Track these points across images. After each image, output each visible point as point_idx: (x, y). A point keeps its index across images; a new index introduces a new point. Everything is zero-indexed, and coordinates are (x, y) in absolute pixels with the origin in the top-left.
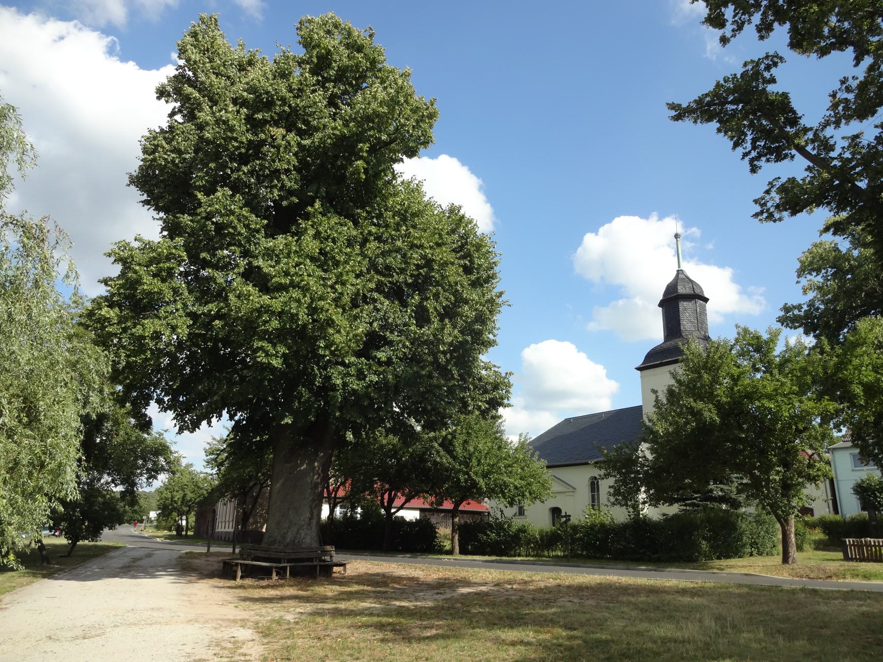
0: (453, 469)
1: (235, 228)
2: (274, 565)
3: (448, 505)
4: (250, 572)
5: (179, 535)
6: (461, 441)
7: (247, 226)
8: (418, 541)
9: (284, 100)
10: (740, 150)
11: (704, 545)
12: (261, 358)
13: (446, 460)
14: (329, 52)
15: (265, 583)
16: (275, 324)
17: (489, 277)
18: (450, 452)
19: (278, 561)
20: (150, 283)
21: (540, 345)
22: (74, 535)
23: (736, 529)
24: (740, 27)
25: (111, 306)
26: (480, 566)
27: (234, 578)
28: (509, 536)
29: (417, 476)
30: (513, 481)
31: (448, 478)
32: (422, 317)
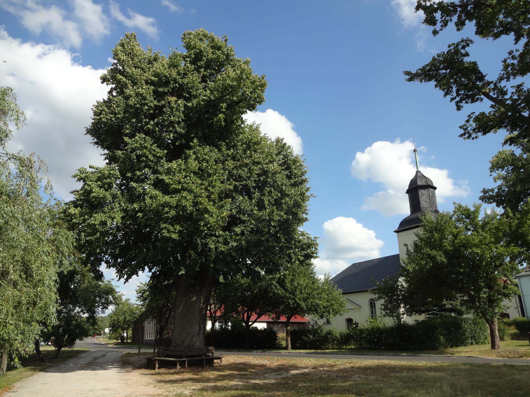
0: (285, 297)
1: (147, 157)
2: (178, 359)
3: (283, 319)
4: (164, 365)
5: (122, 342)
6: (289, 280)
8: (266, 342)
9: (175, 80)
10: (449, 97)
11: (442, 339)
12: (166, 234)
14: (201, 51)
15: (172, 371)
16: (173, 213)
19: (180, 357)
20: (97, 192)
21: (334, 220)
22: (58, 344)
25: (76, 207)
26: (304, 357)
31: (283, 303)
32: (261, 206)
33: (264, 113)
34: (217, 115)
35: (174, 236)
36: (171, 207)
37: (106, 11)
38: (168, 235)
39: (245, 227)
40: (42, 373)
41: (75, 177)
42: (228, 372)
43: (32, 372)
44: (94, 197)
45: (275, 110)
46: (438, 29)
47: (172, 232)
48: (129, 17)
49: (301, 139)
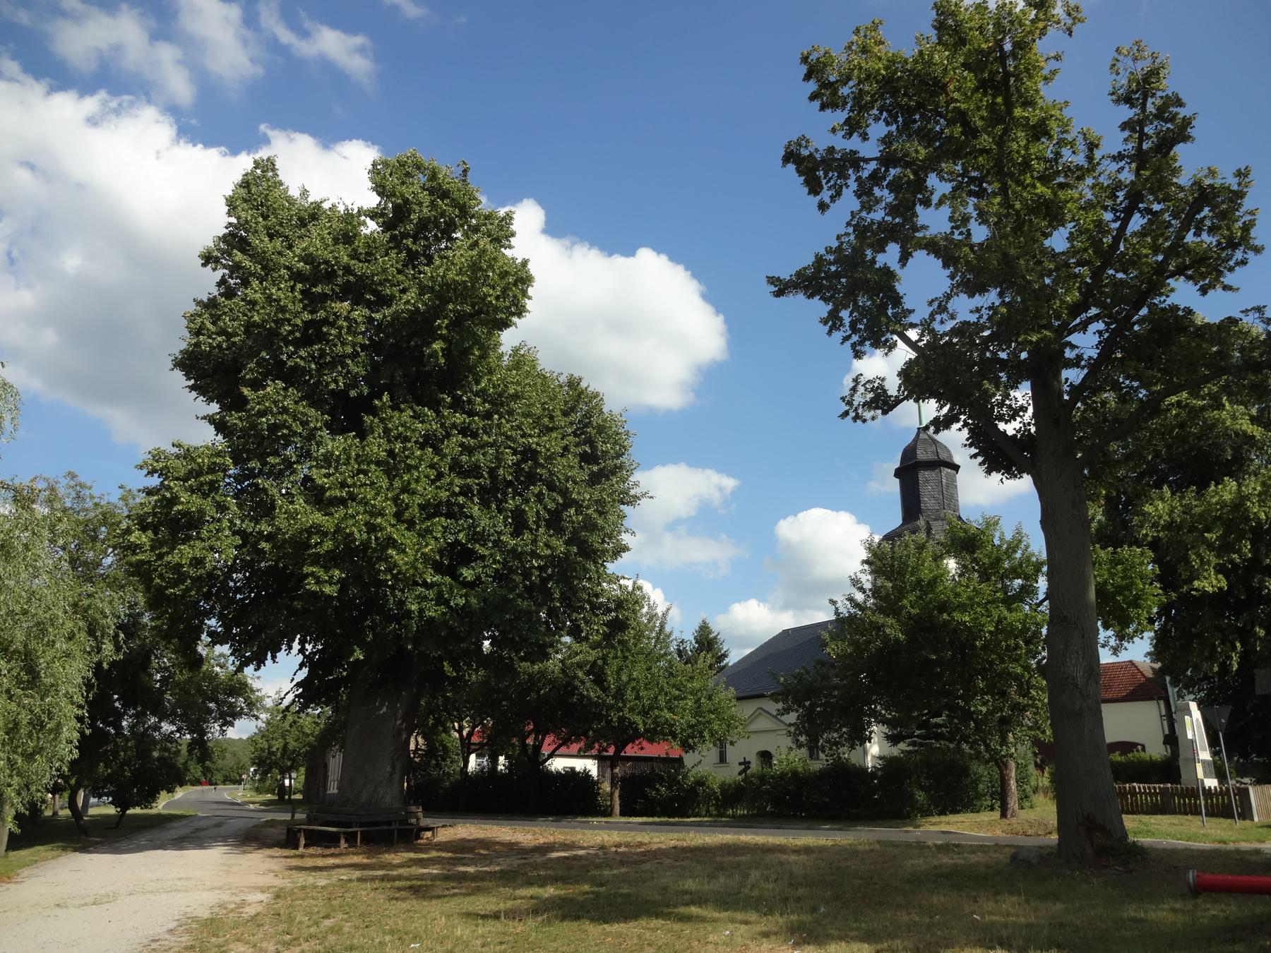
1: (289, 428)
2: (343, 830)
4: (315, 839)
5: (281, 799)
7: (304, 424)
8: (574, 798)
9: (348, 270)
10: (838, 335)
11: (920, 796)
12: (311, 585)
13: (594, 693)
14: (406, 201)
15: (332, 850)
16: (328, 545)
17: (616, 467)
18: (600, 680)
19: (349, 825)
20: (188, 501)
21: (801, 515)
22: (122, 802)
23: (968, 775)
24: (839, 193)
25: (144, 528)
26: (636, 830)
27: (297, 848)
28: (684, 790)
29: (574, 717)
30: (682, 720)
31: (598, 717)
32: (519, 524)
33: (632, 259)
34: (429, 344)
35: (327, 589)
36: (325, 534)
37: (250, 20)
38: (315, 588)
39: (484, 567)
40: (77, 854)
41: (141, 468)
42: (434, 854)
43: (58, 852)
44: (179, 512)
45: (659, 250)
46: (827, 200)
47: (324, 582)
48: (304, 34)
49: (726, 321)
